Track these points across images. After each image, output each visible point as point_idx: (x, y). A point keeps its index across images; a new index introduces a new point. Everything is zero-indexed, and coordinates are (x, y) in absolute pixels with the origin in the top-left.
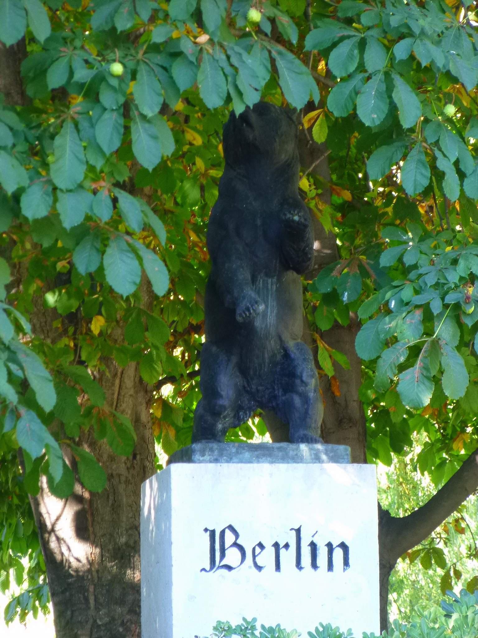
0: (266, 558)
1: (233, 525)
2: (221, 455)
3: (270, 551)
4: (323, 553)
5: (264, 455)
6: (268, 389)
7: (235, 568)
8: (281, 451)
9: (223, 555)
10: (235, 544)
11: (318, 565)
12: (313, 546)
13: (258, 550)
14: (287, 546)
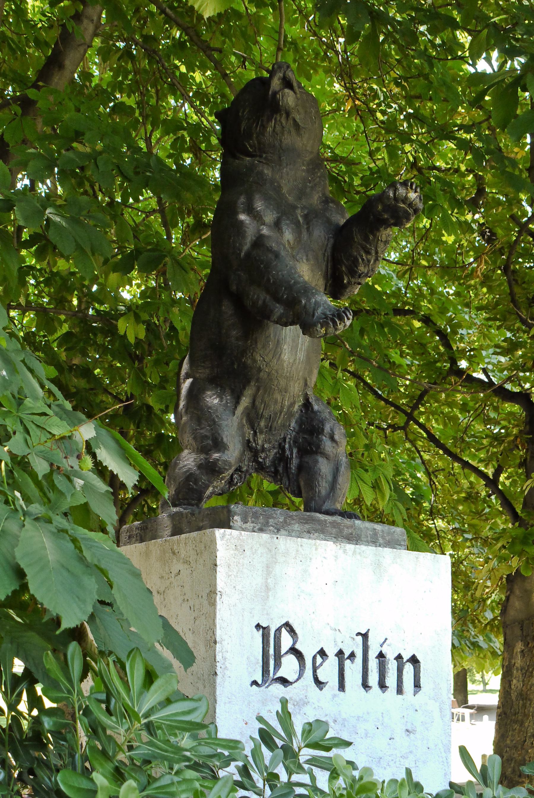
0: (328, 671)
1: (291, 622)
3: (332, 662)
4: (392, 667)
5: (316, 531)
6: (274, 448)
7: (291, 683)
9: (278, 665)
12: (381, 656)
13: (319, 660)
14: (352, 656)
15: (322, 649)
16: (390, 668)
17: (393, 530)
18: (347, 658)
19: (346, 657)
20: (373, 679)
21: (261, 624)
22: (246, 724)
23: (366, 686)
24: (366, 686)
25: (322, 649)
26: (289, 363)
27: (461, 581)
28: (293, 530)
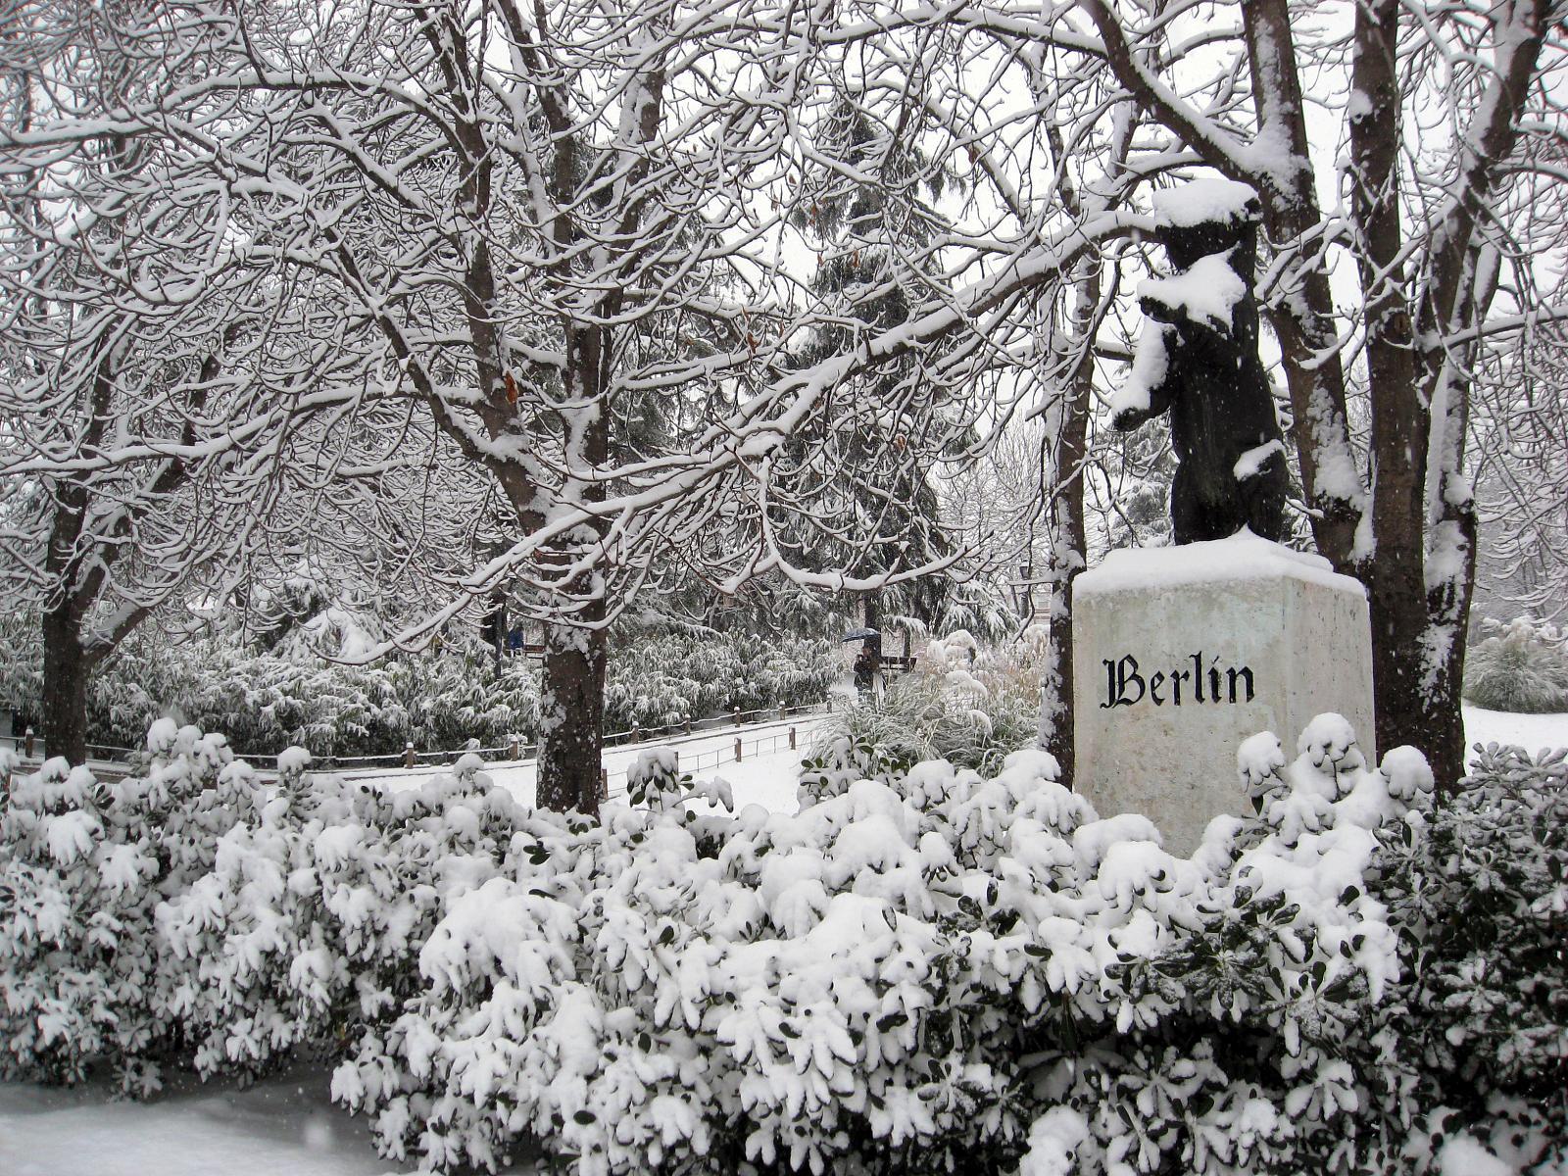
0: (1165, 690)
12: (1214, 673)
14: (1186, 676)
20: (1207, 692)
23: (1199, 697)
24: (1199, 697)
27: (612, 742)
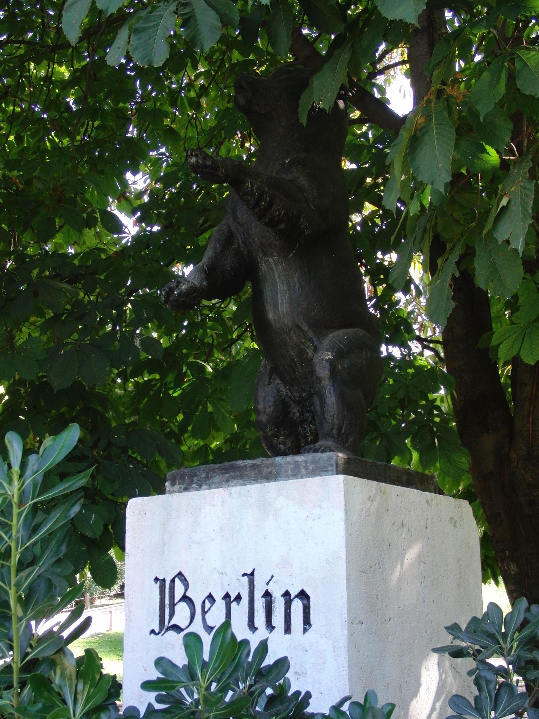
2: (191, 482)
3: (220, 604)
5: (235, 478)
8: (254, 469)
10: (185, 598)
11: (274, 624)
12: (267, 595)
13: (208, 605)
14: (238, 598)
15: (210, 593)
16: (277, 606)
17: (318, 457)
18: (234, 600)
19: (232, 599)
21: (158, 577)
22: (145, 670)
25: (210, 593)
26: (275, 320)
28: (213, 483)
